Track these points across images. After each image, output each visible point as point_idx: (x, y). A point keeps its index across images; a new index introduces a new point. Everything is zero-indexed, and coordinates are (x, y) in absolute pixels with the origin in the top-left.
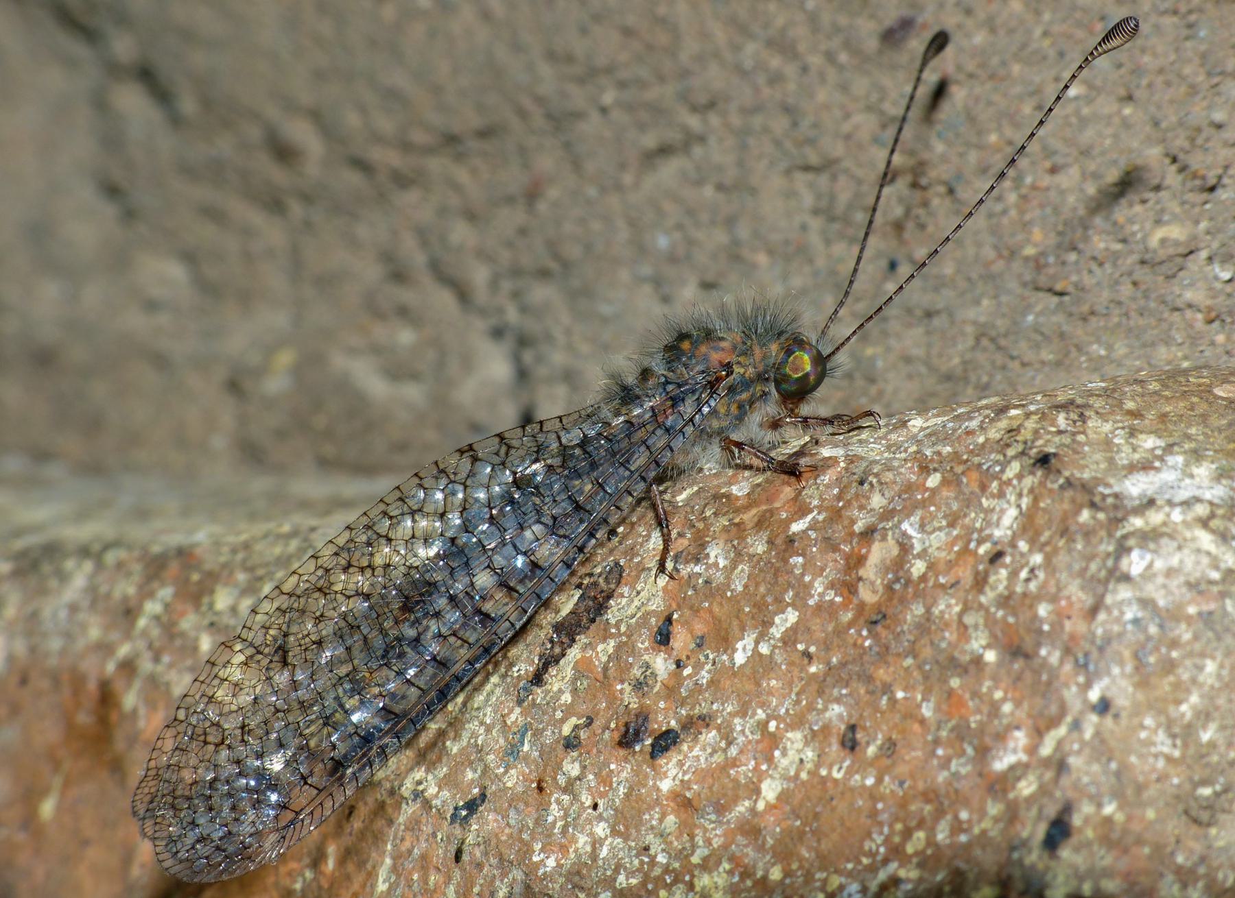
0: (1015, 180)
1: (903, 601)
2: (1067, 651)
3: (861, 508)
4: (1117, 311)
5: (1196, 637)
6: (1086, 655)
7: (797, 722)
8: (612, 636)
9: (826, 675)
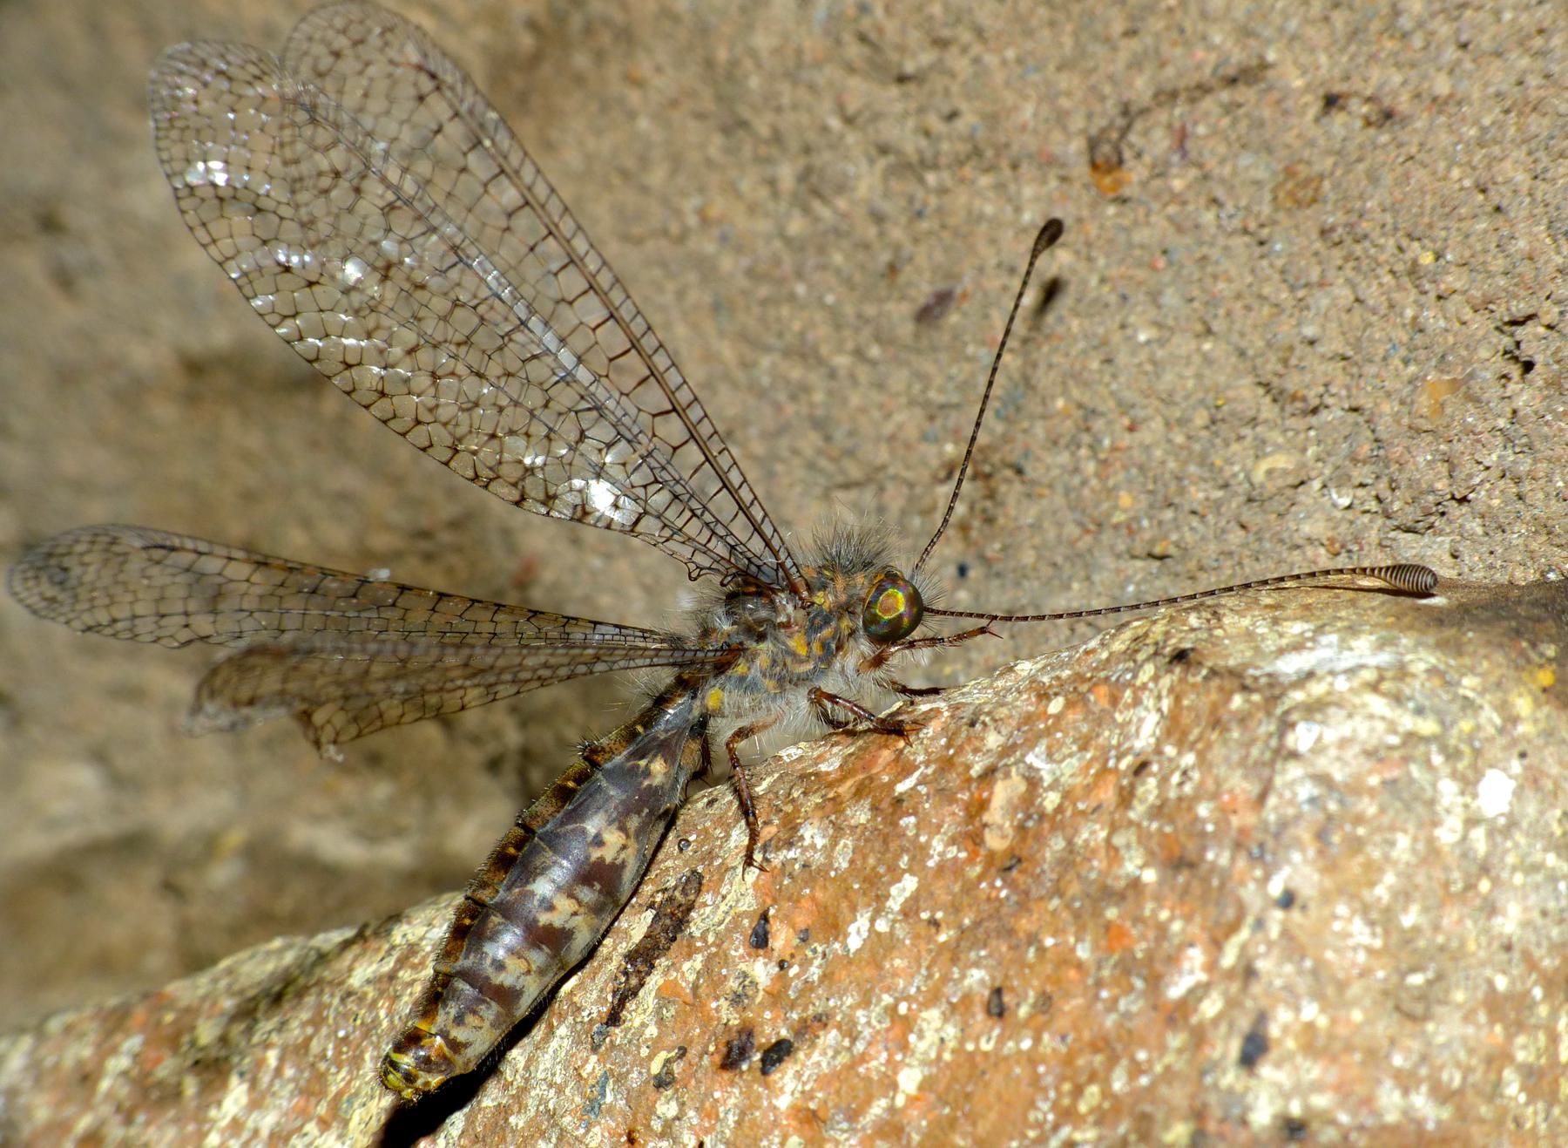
0: (1091, 447)
1: (1039, 838)
2: (1238, 846)
3: (976, 751)
4: (1229, 563)
5: (1383, 810)
6: (1261, 846)
7: (932, 998)
8: (698, 950)
9: (958, 940)
